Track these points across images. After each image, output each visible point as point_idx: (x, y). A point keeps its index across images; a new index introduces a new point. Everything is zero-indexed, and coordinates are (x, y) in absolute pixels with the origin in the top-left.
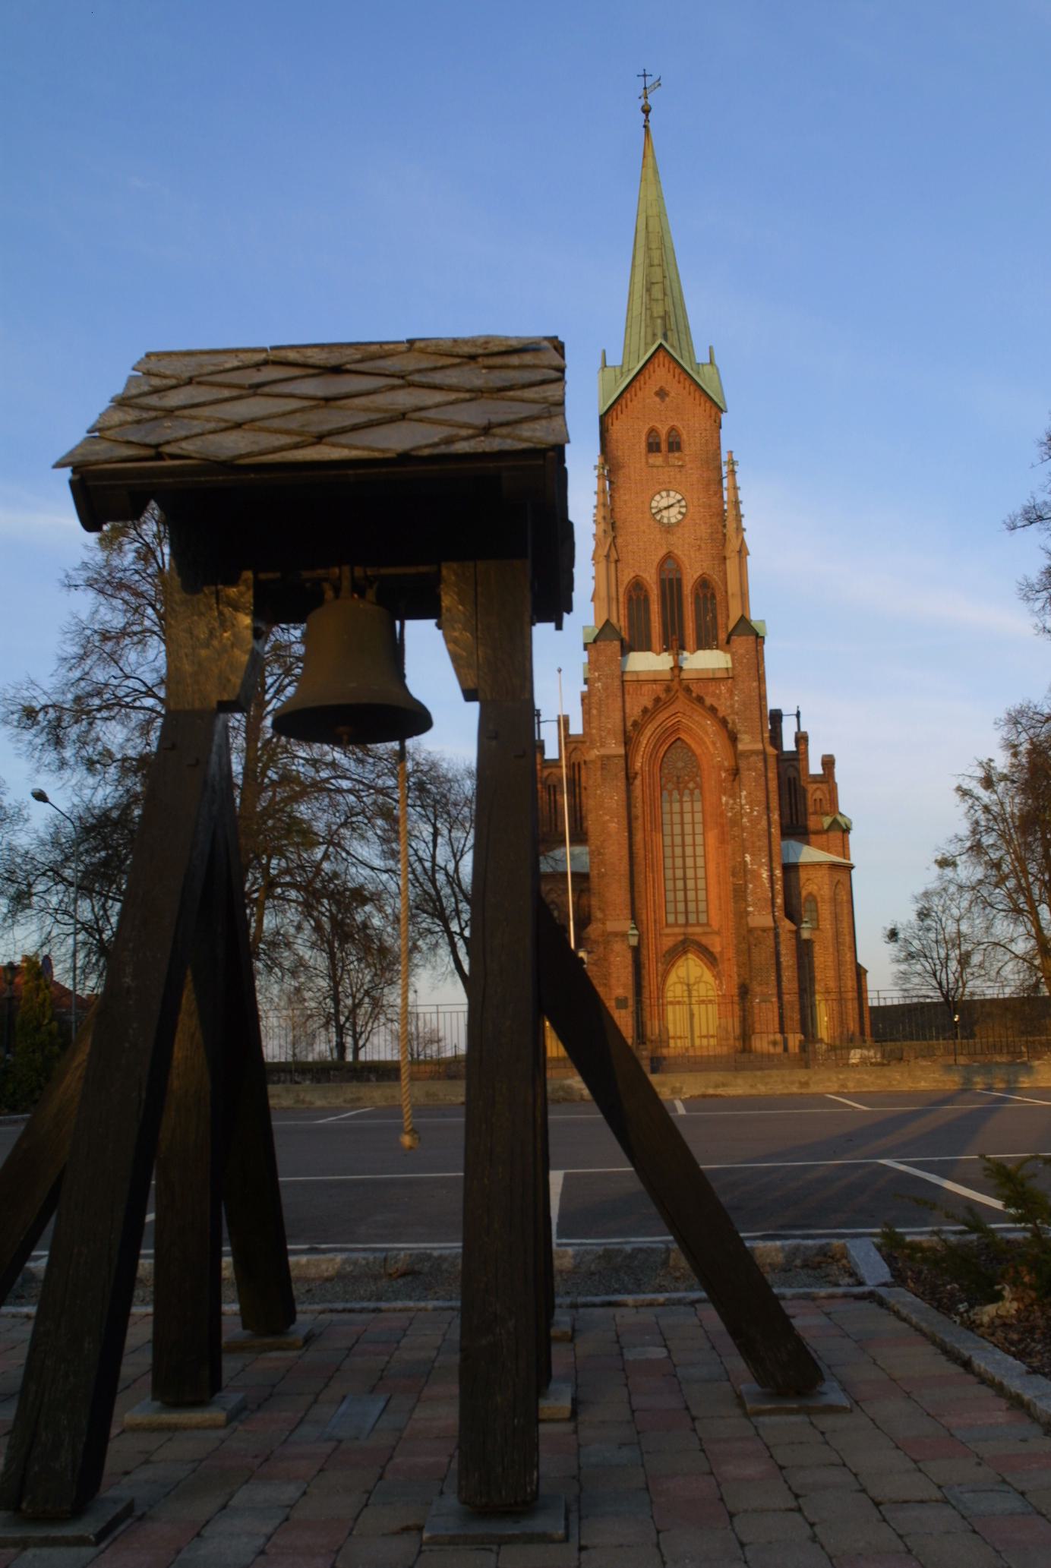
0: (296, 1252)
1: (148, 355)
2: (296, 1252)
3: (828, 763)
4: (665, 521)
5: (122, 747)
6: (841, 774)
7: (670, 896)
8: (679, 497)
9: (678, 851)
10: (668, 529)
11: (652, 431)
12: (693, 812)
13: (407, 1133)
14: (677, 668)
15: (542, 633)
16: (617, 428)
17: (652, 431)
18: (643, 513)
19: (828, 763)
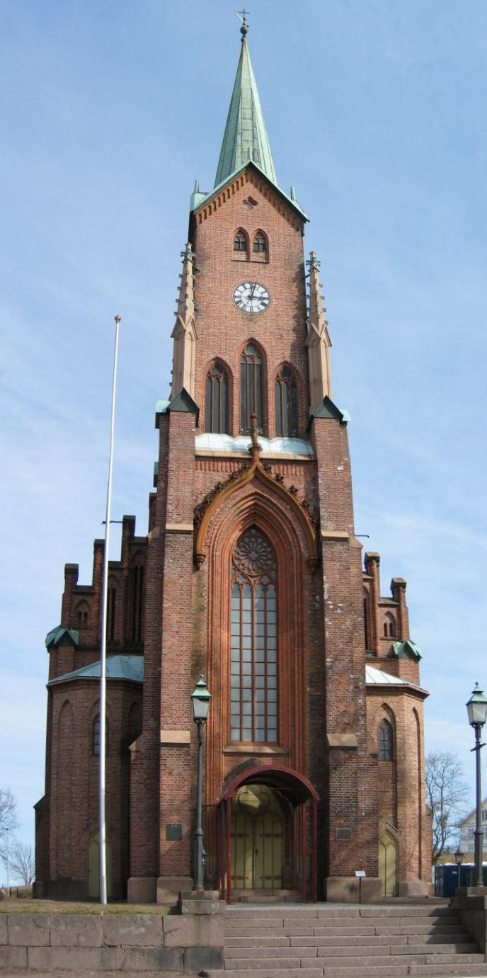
0: (116, 964)
1: (48, 634)
2: (116, 964)
3: (398, 587)
4: (248, 309)
5: (456, 782)
6: (411, 597)
7: (235, 708)
8: (266, 295)
9: (247, 708)
10: (251, 317)
11: (242, 231)
12: (266, 675)
13: (200, 835)
14: (255, 448)
15: (118, 559)
16: (204, 228)
17: (242, 231)
18: (226, 300)
19: (398, 587)
